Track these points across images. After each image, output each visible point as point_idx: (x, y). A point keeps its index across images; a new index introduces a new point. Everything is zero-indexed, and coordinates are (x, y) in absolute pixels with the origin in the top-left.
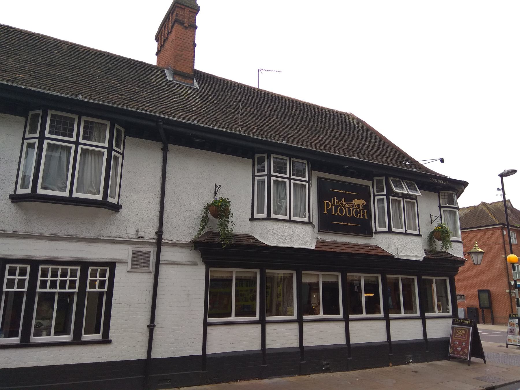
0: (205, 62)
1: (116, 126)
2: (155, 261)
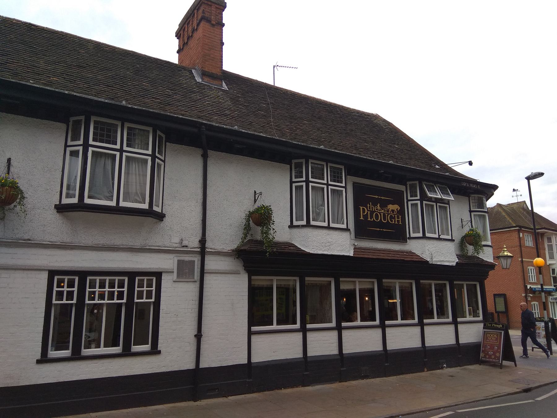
0: (234, 61)
1: (159, 133)
2: (199, 270)
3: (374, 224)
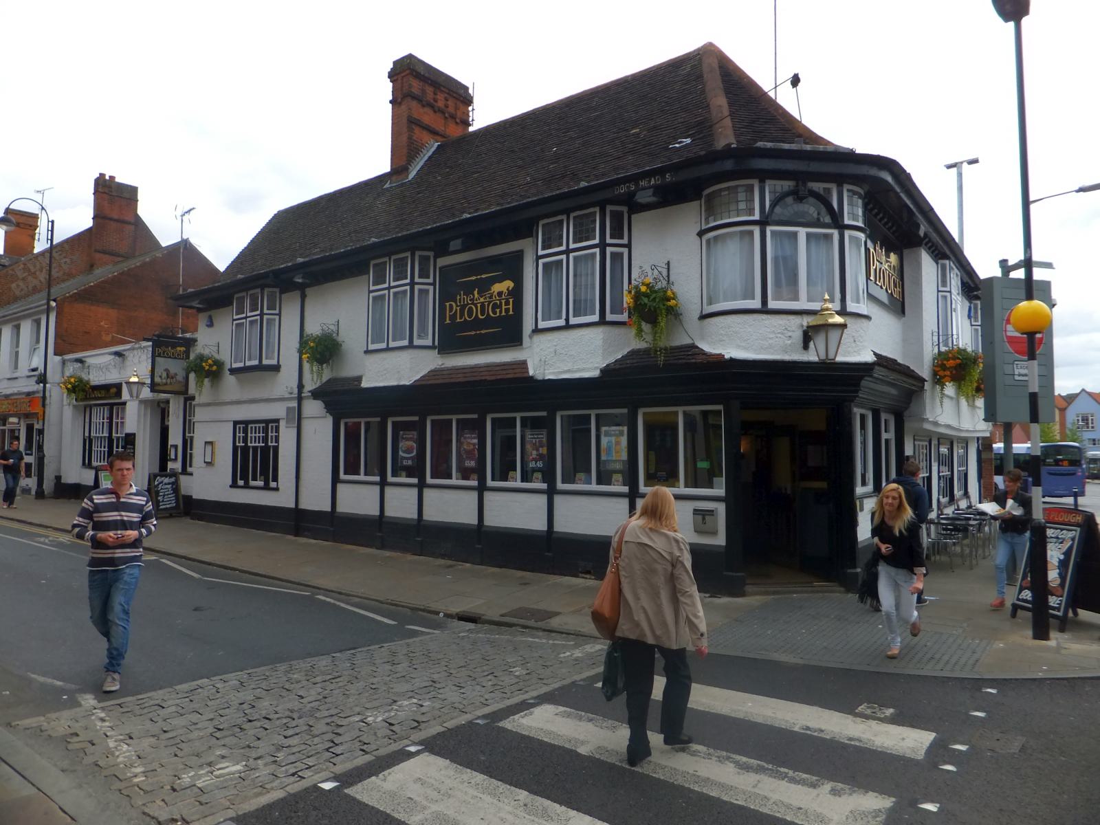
3: (466, 326)
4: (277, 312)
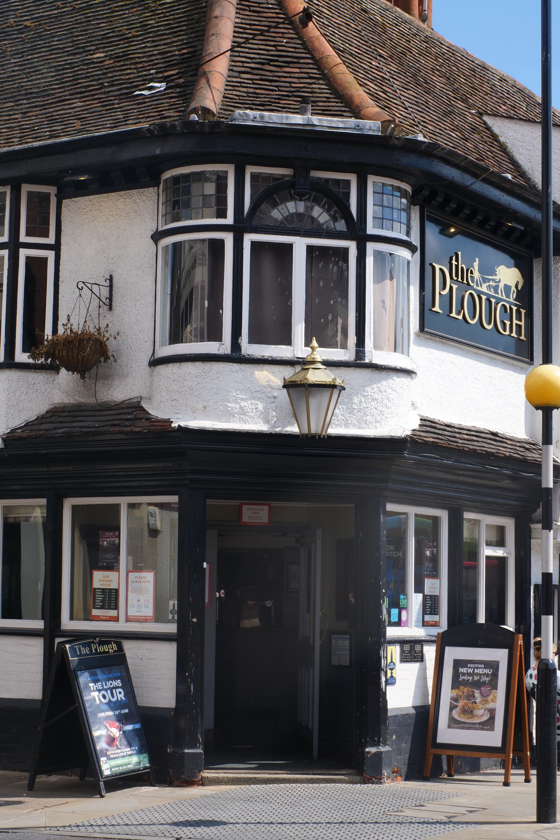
4: (51, 240)
